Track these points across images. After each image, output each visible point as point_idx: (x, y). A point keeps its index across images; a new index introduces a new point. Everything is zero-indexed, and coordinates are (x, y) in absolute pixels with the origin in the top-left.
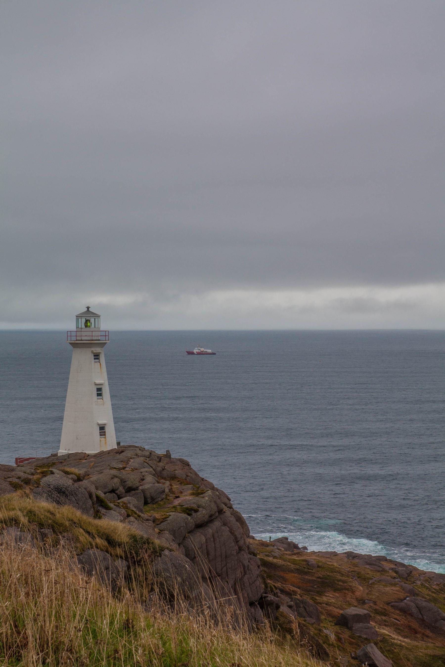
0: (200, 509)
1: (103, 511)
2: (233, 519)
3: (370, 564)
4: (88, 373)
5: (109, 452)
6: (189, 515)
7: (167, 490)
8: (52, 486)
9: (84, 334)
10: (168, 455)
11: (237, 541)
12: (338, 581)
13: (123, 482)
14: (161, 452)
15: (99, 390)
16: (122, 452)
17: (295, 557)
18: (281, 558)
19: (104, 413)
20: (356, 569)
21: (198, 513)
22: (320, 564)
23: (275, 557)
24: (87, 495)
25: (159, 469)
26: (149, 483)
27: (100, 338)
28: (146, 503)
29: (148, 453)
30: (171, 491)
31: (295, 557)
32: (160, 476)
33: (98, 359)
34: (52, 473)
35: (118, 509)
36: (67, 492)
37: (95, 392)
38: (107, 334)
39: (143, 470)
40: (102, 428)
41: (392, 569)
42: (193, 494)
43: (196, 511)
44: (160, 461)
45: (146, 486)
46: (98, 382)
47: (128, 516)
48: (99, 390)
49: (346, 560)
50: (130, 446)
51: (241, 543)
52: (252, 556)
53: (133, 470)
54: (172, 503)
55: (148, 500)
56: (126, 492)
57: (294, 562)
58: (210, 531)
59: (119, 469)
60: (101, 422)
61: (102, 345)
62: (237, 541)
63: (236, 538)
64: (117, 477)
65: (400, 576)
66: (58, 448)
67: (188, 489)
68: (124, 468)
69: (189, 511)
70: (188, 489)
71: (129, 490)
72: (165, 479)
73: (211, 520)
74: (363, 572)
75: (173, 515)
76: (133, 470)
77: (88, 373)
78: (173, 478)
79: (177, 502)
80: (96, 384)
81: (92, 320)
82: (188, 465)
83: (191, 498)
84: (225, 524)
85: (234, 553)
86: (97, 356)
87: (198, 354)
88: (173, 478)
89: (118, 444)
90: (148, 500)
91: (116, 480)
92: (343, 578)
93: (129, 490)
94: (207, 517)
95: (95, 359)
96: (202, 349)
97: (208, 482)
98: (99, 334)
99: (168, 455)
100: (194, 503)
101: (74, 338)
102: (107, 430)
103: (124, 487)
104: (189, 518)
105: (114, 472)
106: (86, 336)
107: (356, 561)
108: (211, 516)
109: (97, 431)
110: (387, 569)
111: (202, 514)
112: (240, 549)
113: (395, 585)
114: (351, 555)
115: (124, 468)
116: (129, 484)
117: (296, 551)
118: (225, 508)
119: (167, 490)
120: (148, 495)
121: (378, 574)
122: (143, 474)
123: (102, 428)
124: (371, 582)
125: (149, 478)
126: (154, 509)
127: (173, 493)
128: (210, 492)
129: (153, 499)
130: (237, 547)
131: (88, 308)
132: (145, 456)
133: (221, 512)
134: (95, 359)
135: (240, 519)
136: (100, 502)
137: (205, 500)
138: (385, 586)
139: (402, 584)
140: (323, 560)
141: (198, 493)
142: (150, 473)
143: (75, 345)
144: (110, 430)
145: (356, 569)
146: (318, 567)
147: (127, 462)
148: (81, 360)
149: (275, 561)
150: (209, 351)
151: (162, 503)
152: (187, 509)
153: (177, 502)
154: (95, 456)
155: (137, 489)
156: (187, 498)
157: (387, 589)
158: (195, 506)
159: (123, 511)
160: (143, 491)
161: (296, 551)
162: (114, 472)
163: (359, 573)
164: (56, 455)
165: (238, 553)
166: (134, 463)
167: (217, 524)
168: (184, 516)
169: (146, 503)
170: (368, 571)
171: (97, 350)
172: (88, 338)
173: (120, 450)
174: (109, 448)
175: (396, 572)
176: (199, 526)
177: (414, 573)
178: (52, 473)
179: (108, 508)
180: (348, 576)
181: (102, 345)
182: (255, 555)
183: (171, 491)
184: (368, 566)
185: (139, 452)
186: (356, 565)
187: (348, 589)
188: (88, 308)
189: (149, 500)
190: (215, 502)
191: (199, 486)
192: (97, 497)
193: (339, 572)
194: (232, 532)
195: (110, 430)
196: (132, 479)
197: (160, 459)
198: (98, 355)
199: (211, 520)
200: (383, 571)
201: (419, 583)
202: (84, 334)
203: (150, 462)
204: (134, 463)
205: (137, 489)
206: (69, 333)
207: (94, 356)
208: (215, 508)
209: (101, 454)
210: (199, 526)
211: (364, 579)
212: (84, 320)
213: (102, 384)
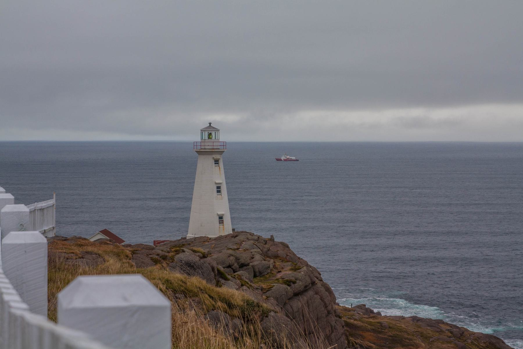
0: (298, 281)
1: (223, 281)
2: (323, 289)
3: (428, 326)
4: (210, 175)
5: (226, 236)
6: (289, 285)
7: (271, 266)
8: (183, 262)
9: (207, 144)
10: (272, 239)
11: (326, 306)
12: (405, 339)
13: (237, 259)
14: (266, 235)
15: (218, 188)
16: (236, 236)
17: (371, 320)
18: (360, 320)
19: (222, 205)
20: (419, 329)
21: (296, 285)
22: (391, 325)
23: (355, 320)
24: (211, 269)
25: (265, 250)
26: (258, 261)
27: (219, 147)
28: (255, 276)
29: (256, 238)
30: (274, 267)
31: (371, 320)
32: (266, 255)
33: (218, 163)
34: (183, 251)
35: (234, 280)
36: (195, 267)
37: (215, 190)
38: (224, 144)
39: (252, 250)
40: (221, 218)
41: (448, 330)
42: (291, 269)
43: (294, 283)
44: (266, 244)
45: (255, 263)
46: (217, 181)
47: (242, 285)
48: (218, 188)
49: (411, 322)
50: (242, 232)
51: (329, 308)
52: (338, 318)
53: (245, 250)
54: (275, 276)
55: (257, 274)
56: (240, 267)
57: (370, 324)
58: (305, 298)
59: (234, 250)
60: (219, 213)
61: (221, 153)
62: (326, 306)
63: (325, 304)
64: (232, 256)
65: (454, 336)
66: (187, 232)
67: (288, 266)
68: (238, 249)
69: (289, 283)
70: (288, 266)
71: (242, 266)
72: (270, 257)
73: (306, 289)
74: (425, 332)
75: (276, 286)
76: (245, 250)
77: (210, 175)
78: (276, 257)
79: (279, 276)
80: (216, 184)
81: (213, 134)
82: (288, 247)
83: (290, 272)
84: (317, 293)
85: (324, 315)
86: (217, 162)
87: (285, 160)
88: (276, 257)
89: (233, 230)
90: (257, 274)
91: (232, 258)
92: (409, 337)
93: (242, 266)
94: (303, 287)
95: (215, 163)
96: (288, 157)
97: (304, 260)
98: (219, 144)
99: (272, 239)
100: (293, 277)
101: (199, 147)
102: (225, 219)
103: (238, 263)
104: (289, 288)
105: (230, 252)
106: (208, 146)
107: (420, 323)
108: (306, 287)
109: (217, 219)
110: (444, 330)
111: (299, 285)
112: (329, 313)
113: (450, 342)
114: (415, 319)
115: (238, 249)
116: (242, 261)
117: (372, 315)
118: (317, 281)
119: (271, 266)
120: (257, 270)
121: (437, 334)
122: (253, 253)
123: (221, 218)
124: (431, 340)
125: (258, 257)
126: (261, 281)
127: (276, 268)
128: (305, 268)
129: (260, 273)
130: (326, 311)
131: (210, 124)
132: (254, 240)
133: (313, 283)
134: (215, 163)
135: (328, 289)
136: (221, 274)
137: (301, 274)
138: (443, 343)
139: (456, 342)
140: (394, 322)
141: (295, 269)
142: (258, 253)
143: (200, 153)
144: (227, 219)
145: (419, 329)
146: (390, 327)
147: (241, 244)
148: (205, 164)
149: (356, 322)
150: (294, 158)
151: (267, 276)
152: (287, 281)
153: (279, 276)
154: (216, 239)
155: (248, 265)
156: (287, 273)
157: (444, 346)
158: (293, 279)
159: (238, 282)
160: (253, 266)
161: (372, 315)
162: (230, 252)
163: (422, 333)
164: (185, 238)
165: (327, 316)
166: (246, 245)
167: (310, 293)
168: (285, 286)
169: (255, 276)
170: (429, 331)
171: (217, 156)
172: (210, 148)
173: (235, 235)
174: (226, 233)
175: (451, 333)
176: (297, 294)
177: (465, 333)
178: (183, 251)
179: (226, 279)
180: (413, 335)
181: (221, 153)
182: (340, 317)
183: (274, 267)
184: (429, 328)
185: (250, 237)
186: (419, 327)
187: (413, 345)
188: (210, 124)
189: (258, 274)
190: (309, 276)
191: (297, 264)
192: (218, 270)
193: (406, 332)
194: (322, 299)
195: (227, 219)
196: (244, 257)
197: (266, 242)
198: (218, 161)
199: (306, 289)
200: (441, 332)
201: (469, 341)
202: (207, 144)
203: (258, 244)
204: (246, 245)
205: (248, 265)
206: (195, 144)
207: (215, 161)
208: (309, 281)
209: (220, 238)
210: (297, 294)
211: (426, 338)
212: (207, 133)
213: (221, 184)
